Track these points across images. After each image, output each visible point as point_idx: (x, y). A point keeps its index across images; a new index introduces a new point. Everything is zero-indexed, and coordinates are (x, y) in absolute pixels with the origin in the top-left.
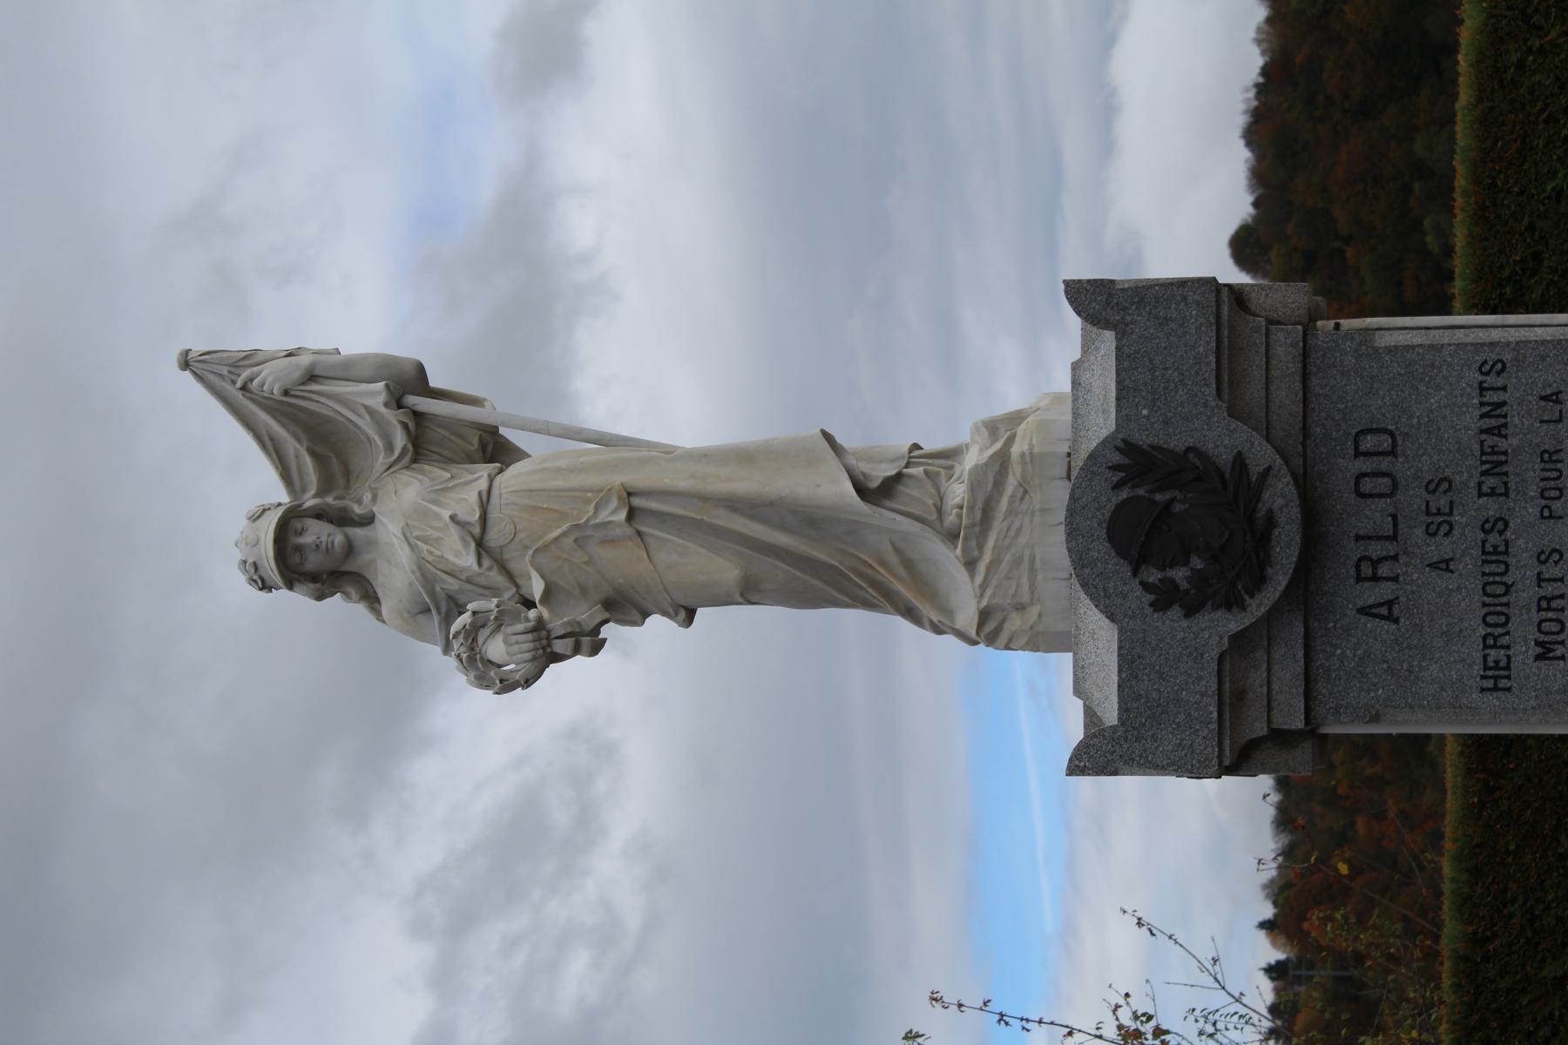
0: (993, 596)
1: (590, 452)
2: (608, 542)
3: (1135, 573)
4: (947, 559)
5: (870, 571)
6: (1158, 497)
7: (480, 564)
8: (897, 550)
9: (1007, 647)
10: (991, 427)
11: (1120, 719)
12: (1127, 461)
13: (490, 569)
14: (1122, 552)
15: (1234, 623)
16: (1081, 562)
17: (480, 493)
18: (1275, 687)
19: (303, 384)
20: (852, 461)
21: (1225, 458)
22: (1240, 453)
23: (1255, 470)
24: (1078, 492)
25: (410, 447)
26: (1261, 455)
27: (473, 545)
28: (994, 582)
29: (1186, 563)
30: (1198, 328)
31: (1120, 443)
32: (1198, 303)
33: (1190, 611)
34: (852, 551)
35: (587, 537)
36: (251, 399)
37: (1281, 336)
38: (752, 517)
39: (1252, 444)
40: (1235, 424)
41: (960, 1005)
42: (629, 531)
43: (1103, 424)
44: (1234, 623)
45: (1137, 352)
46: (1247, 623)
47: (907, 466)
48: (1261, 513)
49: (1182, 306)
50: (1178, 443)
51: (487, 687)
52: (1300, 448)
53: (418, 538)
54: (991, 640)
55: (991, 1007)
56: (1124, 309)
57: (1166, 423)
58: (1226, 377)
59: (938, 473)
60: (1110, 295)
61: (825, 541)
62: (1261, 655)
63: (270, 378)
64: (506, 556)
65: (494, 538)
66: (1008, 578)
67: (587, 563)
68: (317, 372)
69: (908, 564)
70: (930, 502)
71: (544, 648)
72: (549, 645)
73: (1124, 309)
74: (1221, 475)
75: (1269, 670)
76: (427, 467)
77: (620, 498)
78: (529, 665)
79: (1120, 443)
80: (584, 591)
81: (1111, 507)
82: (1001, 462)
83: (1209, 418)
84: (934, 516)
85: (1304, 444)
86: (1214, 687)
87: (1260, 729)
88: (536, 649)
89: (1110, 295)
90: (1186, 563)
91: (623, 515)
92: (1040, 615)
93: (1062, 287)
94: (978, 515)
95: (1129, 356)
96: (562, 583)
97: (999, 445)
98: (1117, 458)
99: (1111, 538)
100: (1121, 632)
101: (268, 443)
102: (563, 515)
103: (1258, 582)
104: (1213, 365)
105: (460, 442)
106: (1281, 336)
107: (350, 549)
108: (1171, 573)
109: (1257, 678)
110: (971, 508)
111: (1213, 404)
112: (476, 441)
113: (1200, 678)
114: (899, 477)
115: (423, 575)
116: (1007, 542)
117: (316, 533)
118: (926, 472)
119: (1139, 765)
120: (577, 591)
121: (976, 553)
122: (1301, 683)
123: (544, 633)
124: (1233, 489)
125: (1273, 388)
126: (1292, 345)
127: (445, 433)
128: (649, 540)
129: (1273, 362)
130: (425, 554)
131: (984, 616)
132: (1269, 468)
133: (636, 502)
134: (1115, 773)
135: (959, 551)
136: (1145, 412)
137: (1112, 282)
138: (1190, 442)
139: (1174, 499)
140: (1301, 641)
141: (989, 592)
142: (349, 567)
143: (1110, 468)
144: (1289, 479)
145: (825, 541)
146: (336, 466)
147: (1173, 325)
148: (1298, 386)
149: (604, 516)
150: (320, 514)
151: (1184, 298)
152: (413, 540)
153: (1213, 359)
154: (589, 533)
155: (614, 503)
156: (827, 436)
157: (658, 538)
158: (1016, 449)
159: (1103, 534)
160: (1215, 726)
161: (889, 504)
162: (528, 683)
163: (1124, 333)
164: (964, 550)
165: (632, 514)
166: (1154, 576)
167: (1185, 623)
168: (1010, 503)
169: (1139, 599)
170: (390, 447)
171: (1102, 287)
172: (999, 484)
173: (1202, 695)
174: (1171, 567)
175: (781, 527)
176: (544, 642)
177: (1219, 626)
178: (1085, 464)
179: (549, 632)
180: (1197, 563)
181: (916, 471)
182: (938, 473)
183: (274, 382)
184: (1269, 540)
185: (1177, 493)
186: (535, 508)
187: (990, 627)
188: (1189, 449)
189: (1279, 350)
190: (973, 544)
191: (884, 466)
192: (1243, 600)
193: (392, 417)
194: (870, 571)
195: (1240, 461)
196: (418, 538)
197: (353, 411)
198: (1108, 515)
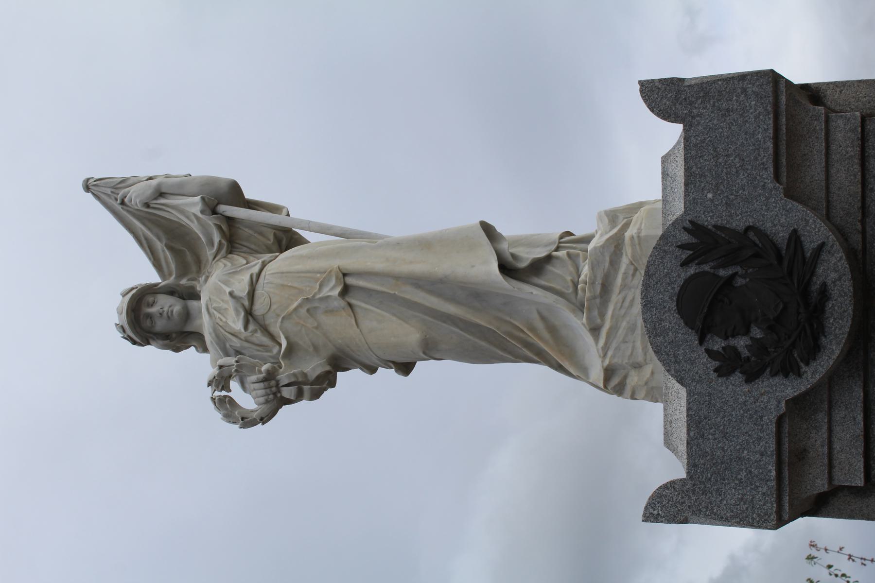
0: (613, 356)
1: (336, 241)
2: (330, 312)
3: (701, 342)
4: (576, 324)
5: (522, 335)
6: (722, 273)
7: (246, 327)
8: (543, 318)
9: (633, 397)
10: (612, 216)
11: (688, 473)
12: (694, 241)
13: (255, 331)
14: (689, 323)
15: (791, 388)
16: (654, 331)
17: (251, 276)
18: (837, 446)
19: (156, 199)
20: (504, 246)
21: (781, 236)
22: (795, 231)
23: (809, 246)
24: (652, 269)
25: (224, 242)
26: (816, 232)
27: (243, 314)
28: (614, 345)
29: (747, 332)
30: (757, 117)
31: (687, 224)
32: (757, 94)
33: (751, 377)
34: (508, 319)
35: (315, 308)
36: (128, 211)
37: (840, 122)
38: (431, 292)
39: (807, 222)
40: (791, 204)
41: (826, 550)
42: (342, 303)
43: (678, 208)
44: (791, 388)
45: (703, 141)
46: (803, 389)
47: (557, 250)
48: (815, 287)
49: (742, 98)
50: (739, 223)
51: (234, 423)
52: (859, 227)
53: (215, 309)
54: (619, 390)
55: (844, 551)
56: (691, 103)
57: (728, 205)
58: (784, 161)
59: (578, 255)
60: (679, 92)
61: (494, 308)
62: (822, 417)
63: (136, 195)
64: (267, 322)
65: (259, 308)
66: (624, 341)
67: (316, 328)
68: (164, 190)
69: (553, 330)
70: (569, 278)
71: (275, 394)
72: (280, 392)
73: (691, 103)
74: (778, 251)
75: (830, 430)
76: (235, 256)
77: (337, 278)
78: (264, 406)
79: (687, 224)
80: (316, 349)
81: (680, 282)
82: (616, 244)
83: (767, 199)
84: (571, 290)
85: (863, 222)
86: (773, 446)
87: (821, 485)
88: (268, 395)
89: (679, 92)
90: (747, 332)
91: (339, 289)
92: (652, 373)
93: (638, 87)
94: (598, 288)
95: (696, 145)
96: (301, 343)
97: (615, 231)
98: (685, 238)
99: (680, 310)
100: (690, 394)
101: (144, 242)
102: (301, 291)
103: (813, 351)
104: (771, 151)
105: (260, 237)
106: (840, 122)
107: (187, 316)
108: (733, 342)
109: (817, 441)
110: (593, 283)
111: (771, 186)
112: (272, 237)
113: (760, 439)
114: (549, 258)
115: (217, 336)
116: (623, 311)
117: (166, 304)
118: (569, 254)
119: (706, 515)
120: (311, 349)
121: (599, 321)
122: (861, 444)
123: (273, 383)
124: (791, 263)
125: (833, 171)
126: (853, 130)
127: (251, 232)
128: (358, 310)
129: (833, 147)
130: (218, 321)
131: (609, 373)
132: (823, 244)
133: (350, 280)
134: (686, 521)
135: (584, 320)
136: (710, 196)
137: (682, 80)
138: (751, 222)
139: (736, 273)
140: (860, 404)
141: (610, 353)
142: (189, 328)
143: (679, 247)
144: (841, 254)
145: (494, 308)
146: (189, 258)
147: (735, 116)
148: (857, 168)
149: (325, 292)
150: (171, 291)
151: (744, 90)
152: (212, 310)
153: (770, 145)
154: (316, 304)
155: (333, 282)
156: (488, 230)
157: (366, 309)
158: (628, 234)
159: (673, 306)
160: (773, 484)
161: (536, 280)
162: (264, 420)
163: (691, 125)
164: (588, 318)
165: (346, 290)
166: (718, 344)
167: (746, 388)
168: (624, 279)
169: (705, 365)
170: (211, 242)
171: (674, 85)
172: (614, 263)
173: (762, 454)
174: (733, 336)
175: (453, 300)
176: (274, 389)
177: (776, 392)
178: (658, 244)
179: (278, 382)
180: (757, 333)
181: (562, 254)
182: (578, 255)
183: (136, 197)
184: (823, 311)
185: (738, 269)
186: (283, 285)
187: (615, 381)
188: (748, 229)
189: (839, 136)
190: (596, 313)
191: (538, 250)
192: (799, 368)
193: (210, 221)
194: (522, 335)
195: (795, 238)
196: (215, 309)
197: (188, 218)
198: (677, 289)
